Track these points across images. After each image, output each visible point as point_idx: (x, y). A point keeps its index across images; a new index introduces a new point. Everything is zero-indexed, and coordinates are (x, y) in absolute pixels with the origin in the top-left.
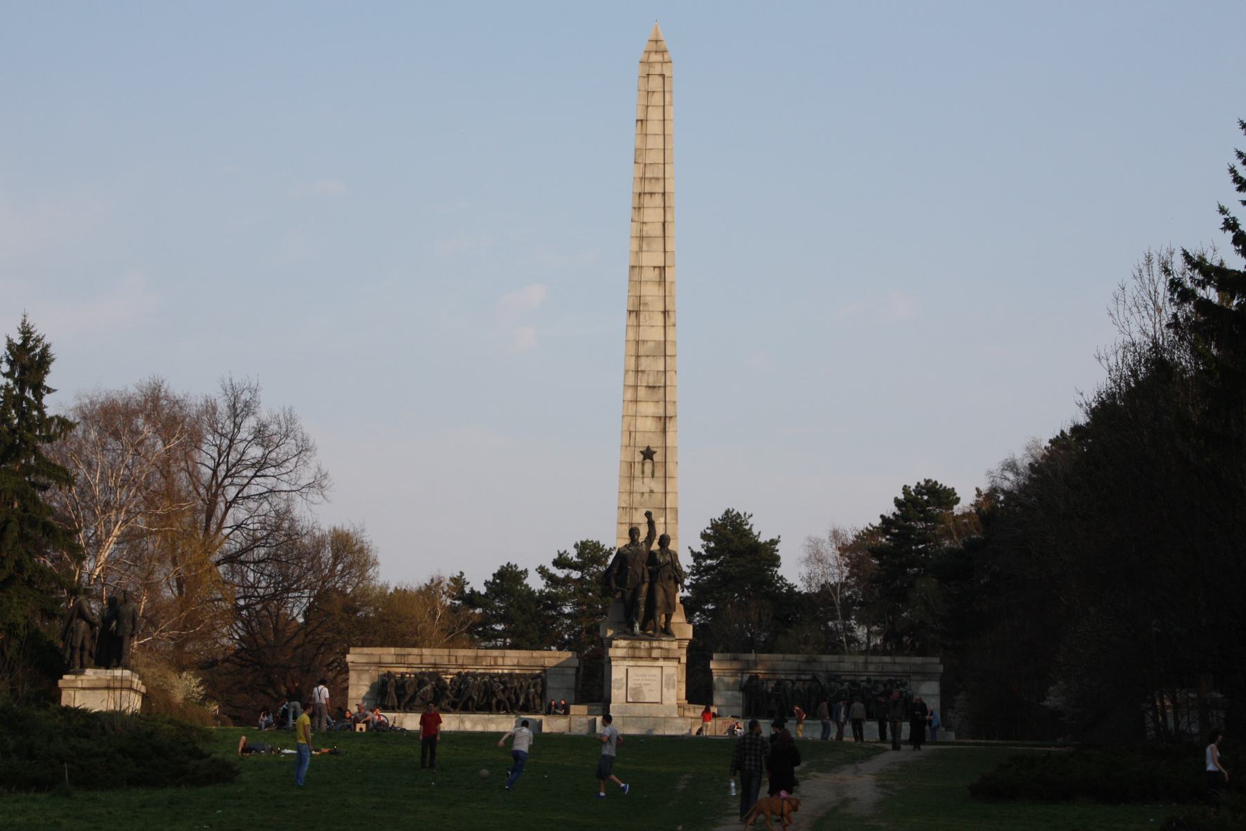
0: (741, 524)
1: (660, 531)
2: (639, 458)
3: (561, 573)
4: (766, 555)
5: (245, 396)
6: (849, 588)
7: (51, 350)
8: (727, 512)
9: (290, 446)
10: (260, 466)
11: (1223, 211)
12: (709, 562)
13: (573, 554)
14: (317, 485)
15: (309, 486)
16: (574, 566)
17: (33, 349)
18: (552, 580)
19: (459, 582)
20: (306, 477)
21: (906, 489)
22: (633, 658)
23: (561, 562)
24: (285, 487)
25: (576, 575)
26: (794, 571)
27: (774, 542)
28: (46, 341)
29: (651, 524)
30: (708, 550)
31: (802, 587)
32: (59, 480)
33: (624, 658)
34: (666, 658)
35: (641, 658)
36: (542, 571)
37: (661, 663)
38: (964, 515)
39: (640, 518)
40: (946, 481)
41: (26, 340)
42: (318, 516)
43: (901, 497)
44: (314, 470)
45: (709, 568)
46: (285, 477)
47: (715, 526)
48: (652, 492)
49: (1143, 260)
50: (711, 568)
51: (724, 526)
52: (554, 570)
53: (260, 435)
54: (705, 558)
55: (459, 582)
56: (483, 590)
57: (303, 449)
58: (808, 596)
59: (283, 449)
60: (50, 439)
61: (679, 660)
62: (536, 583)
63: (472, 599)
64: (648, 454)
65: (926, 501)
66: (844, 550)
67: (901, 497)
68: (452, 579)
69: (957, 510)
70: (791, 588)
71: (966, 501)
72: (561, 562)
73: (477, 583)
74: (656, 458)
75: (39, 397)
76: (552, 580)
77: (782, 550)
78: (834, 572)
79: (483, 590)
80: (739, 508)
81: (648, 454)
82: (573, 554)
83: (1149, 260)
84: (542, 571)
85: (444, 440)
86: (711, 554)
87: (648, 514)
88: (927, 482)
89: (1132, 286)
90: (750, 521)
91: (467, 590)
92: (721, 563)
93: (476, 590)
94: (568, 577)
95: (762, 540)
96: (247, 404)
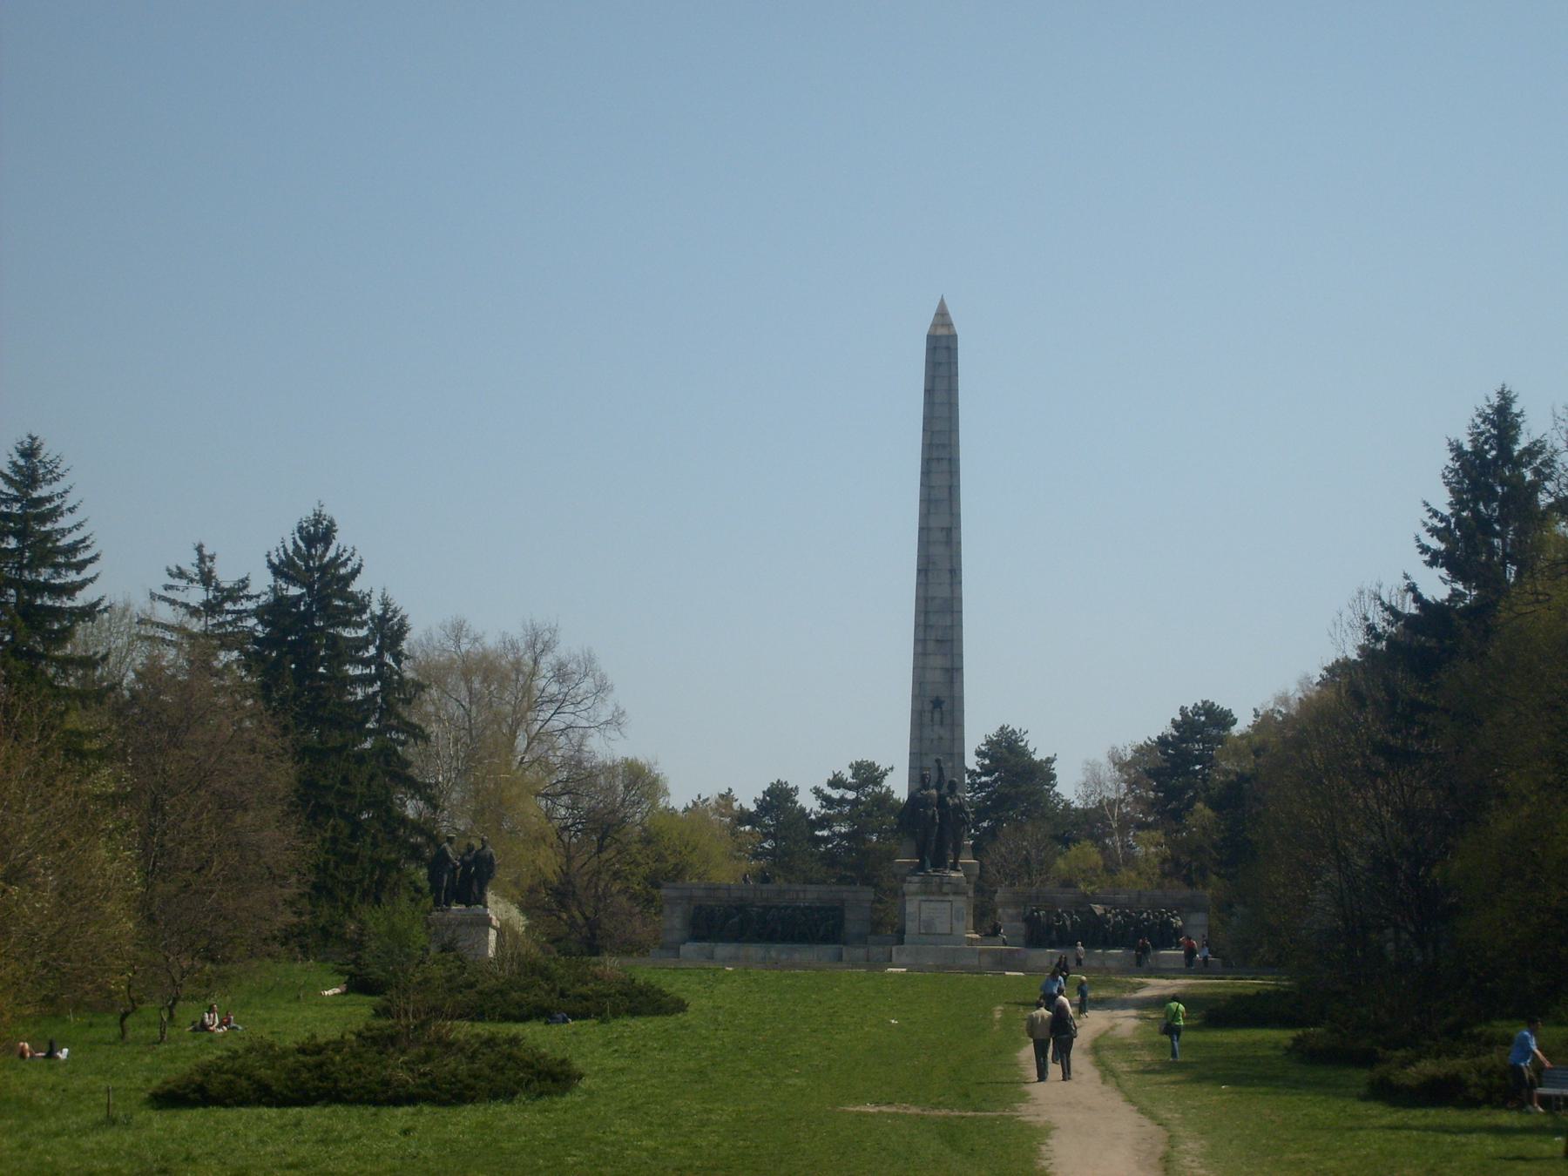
0: (1016, 741)
1: (948, 775)
2: (928, 707)
3: (836, 794)
4: (1042, 773)
5: (547, 636)
6: (1127, 805)
7: (408, 621)
8: (1002, 728)
9: (587, 684)
10: (559, 703)
11: (1406, 577)
12: (984, 779)
13: (848, 775)
14: (616, 721)
15: (607, 723)
16: (849, 787)
17: (391, 619)
18: (828, 801)
19: (727, 798)
20: (605, 713)
21: (1183, 710)
22: (925, 893)
23: (836, 782)
24: (584, 723)
25: (851, 795)
26: (1070, 787)
27: (1050, 761)
28: (403, 612)
29: (940, 770)
30: (982, 766)
31: (1078, 804)
32: (416, 737)
33: (916, 894)
34: (955, 893)
35: (933, 893)
36: (818, 792)
37: (951, 898)
38: (1242, 737)
39: (929, 762)
40: (1223, 703)
41: (385, 611)
42: (605, 749)
43: (1179, 718)
44: (612, 708)
45: (983, 786)
46: (584, 714)
47: (989, 742)
48: (941, 738)
49: (1356, 594)
50: (985, 784)
51: (998, 743)
52: (828, 791)
53: (561, 674)
54: (979, 775)
55: (727, 798)
56: (753, 808)
57: (602, 688)
58: (1085, 813)
59: (584, 686)
60: (408, 702)
61: (965, 893)
62: (808, 803)
63: (744, 817)
64: (937, 703)
65: (1202, 725)
66: (1122, 766)
67: (1179, 718)
68: (721, 796)
69: (1236, 730)
70: (1067, 805)
71: (1244, 723)
72: (836, 782)
73: (747, 800)
74: (945, 707)
75: (398, 662)
76: (828, 801)
77: (1058, 768)
78: (1113, 788)
79: (753, 808)
80: (1014, 725)
81: (937, 703)
82: (848, 775)
83: (1361, 593)
84: (818, 792)
85: (721, 668)
86: (986, 771)
87: (938, 761)
88: (1204, 703)
89: (1348, 613)
90: (1026, 737)
91: (736, 805)
92: (995, 781)
93: (745, 806)
94: (842, 797)
95: (1037, 757)
96: (546, 644)
